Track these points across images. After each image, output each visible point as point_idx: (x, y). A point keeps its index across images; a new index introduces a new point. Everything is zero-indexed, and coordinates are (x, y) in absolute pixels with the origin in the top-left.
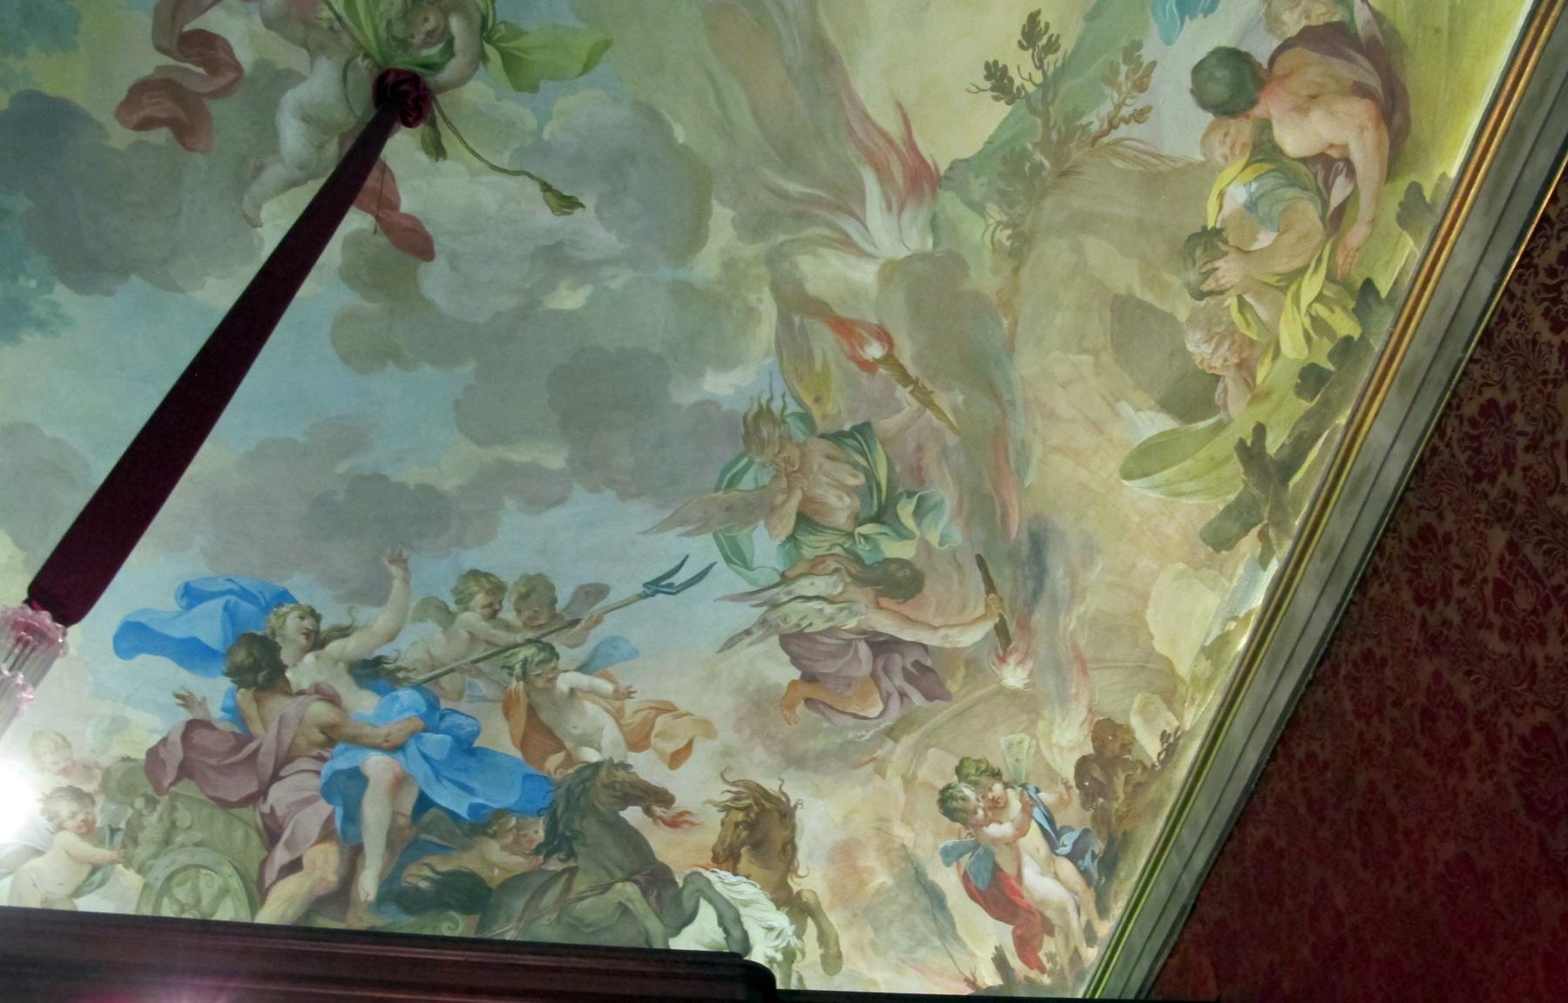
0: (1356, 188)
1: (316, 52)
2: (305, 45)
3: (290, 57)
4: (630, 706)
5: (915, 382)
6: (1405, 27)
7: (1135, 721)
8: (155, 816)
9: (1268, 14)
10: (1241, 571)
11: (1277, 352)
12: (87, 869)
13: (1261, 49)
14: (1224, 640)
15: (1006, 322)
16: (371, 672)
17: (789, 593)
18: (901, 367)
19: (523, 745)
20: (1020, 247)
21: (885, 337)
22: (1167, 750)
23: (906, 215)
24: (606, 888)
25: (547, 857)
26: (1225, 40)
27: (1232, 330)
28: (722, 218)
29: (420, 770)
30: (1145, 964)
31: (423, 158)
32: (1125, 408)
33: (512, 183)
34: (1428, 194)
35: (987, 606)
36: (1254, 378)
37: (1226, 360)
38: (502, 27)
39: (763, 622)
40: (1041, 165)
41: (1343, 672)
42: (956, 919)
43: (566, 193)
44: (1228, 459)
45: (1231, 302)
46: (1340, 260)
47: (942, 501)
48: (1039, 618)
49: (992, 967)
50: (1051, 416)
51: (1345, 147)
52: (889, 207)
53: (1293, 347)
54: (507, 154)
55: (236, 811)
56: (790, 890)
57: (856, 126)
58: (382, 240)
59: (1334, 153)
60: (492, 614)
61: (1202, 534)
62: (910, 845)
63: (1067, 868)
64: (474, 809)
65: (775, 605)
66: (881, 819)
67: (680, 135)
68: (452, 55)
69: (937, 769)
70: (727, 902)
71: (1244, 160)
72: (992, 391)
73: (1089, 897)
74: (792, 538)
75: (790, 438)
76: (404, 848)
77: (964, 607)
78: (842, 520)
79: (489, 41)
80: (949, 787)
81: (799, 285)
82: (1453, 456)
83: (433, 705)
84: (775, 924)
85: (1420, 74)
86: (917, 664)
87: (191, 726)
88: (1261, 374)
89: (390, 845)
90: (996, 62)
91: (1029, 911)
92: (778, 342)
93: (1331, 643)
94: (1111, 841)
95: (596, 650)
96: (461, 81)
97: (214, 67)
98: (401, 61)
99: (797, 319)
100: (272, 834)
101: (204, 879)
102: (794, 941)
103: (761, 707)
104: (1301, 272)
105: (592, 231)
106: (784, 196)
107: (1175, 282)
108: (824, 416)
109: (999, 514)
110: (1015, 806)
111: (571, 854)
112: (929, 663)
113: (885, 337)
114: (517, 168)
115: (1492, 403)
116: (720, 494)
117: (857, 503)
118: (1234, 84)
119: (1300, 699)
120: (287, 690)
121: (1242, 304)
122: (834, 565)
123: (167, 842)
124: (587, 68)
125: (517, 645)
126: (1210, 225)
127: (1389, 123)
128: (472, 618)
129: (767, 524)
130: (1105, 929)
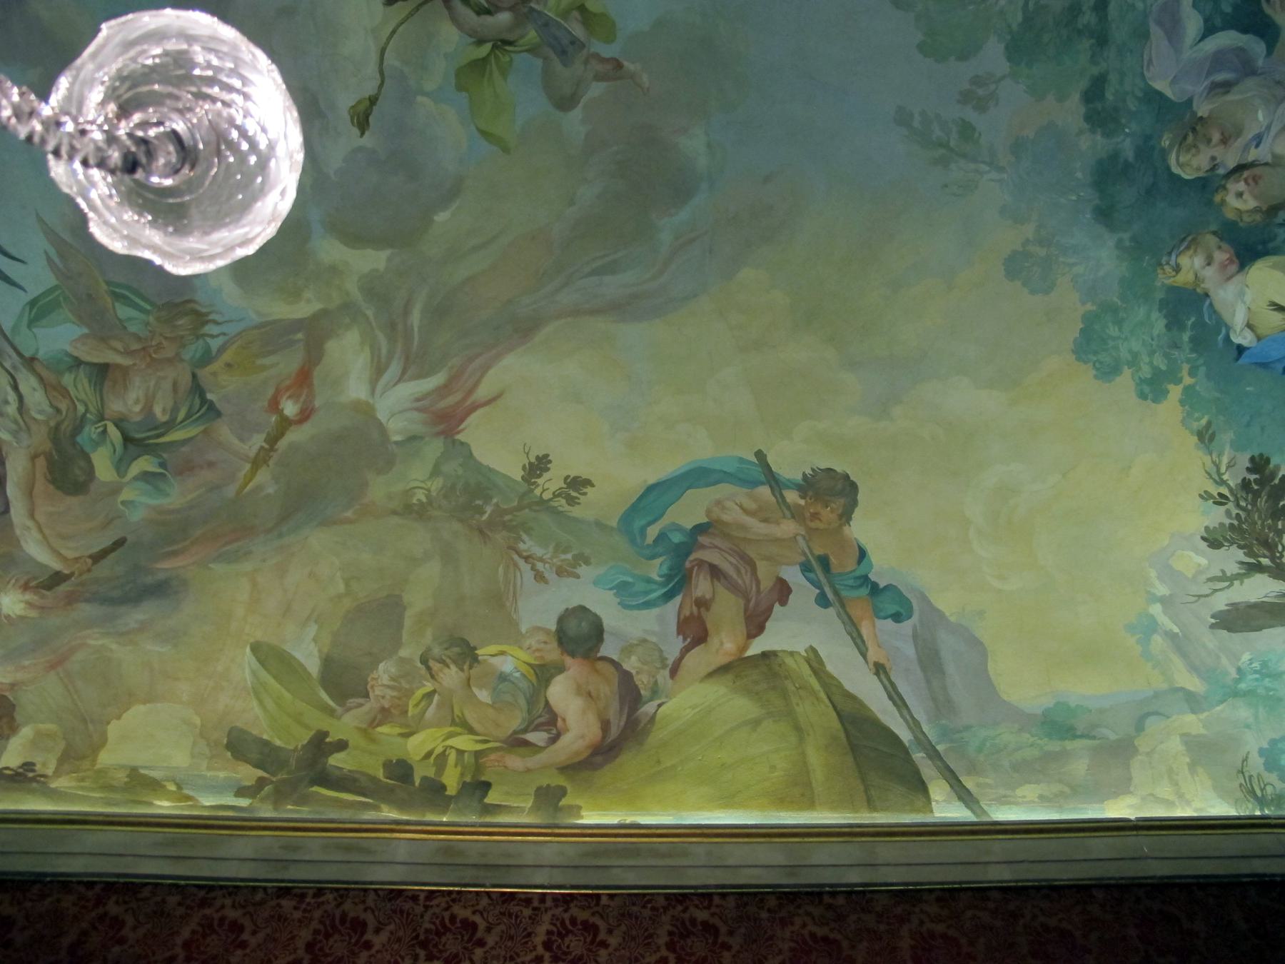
0: (545, 748)
5: (272, 449)
7: (26, 732)
9: (632, 646)
10: (222, 774)
11: (407, 735)
13: (609, 649)
14: (155, 786)
15: (349, 514)
17: (14, 367)
18: (282, 434)
20: (415, 512)
21: (305, 415)
22: (18, 774)
23: (416, 415)
26: (607, 622)
27: (409, 693)
28: (373, 260)
32: (312, 629)
33: (371, 68)
34: (563, 802)
35: (77, 560)
36: (379, 725)
37: (383, 697)
38: (508, 59)
41: (207, 911)
43: (371, 119)
44: (307, 727)
45: (429, 686)
46: (493, 757)
47: (168, 495)
51: (567, 730)
52: (418, 400)
53: (417, 746)
54: (397, 64)
59: (560, 723)
67: (441, 217)
71: (533, 662)
74: (78, 363)
75: (184, 346)
78: (115, 406)
82: (422, 916)
85: (630, 763)
88: (384, 729)
90: (550, 462)
92: (274, 322)
93: (221, 887)
96: (455, 20)
99: (300, 336)
104: (471, 731)
106: (406, 312)
108: (214, 374)
109: (175, 547)
115: (474, 926)
116: (104, 287)
117: (138, 419)
118: (580, 637)
119: (157, 886)
121: (430, 695)
122: (63, 406)
124: (484, 133)
129: (85, 336)
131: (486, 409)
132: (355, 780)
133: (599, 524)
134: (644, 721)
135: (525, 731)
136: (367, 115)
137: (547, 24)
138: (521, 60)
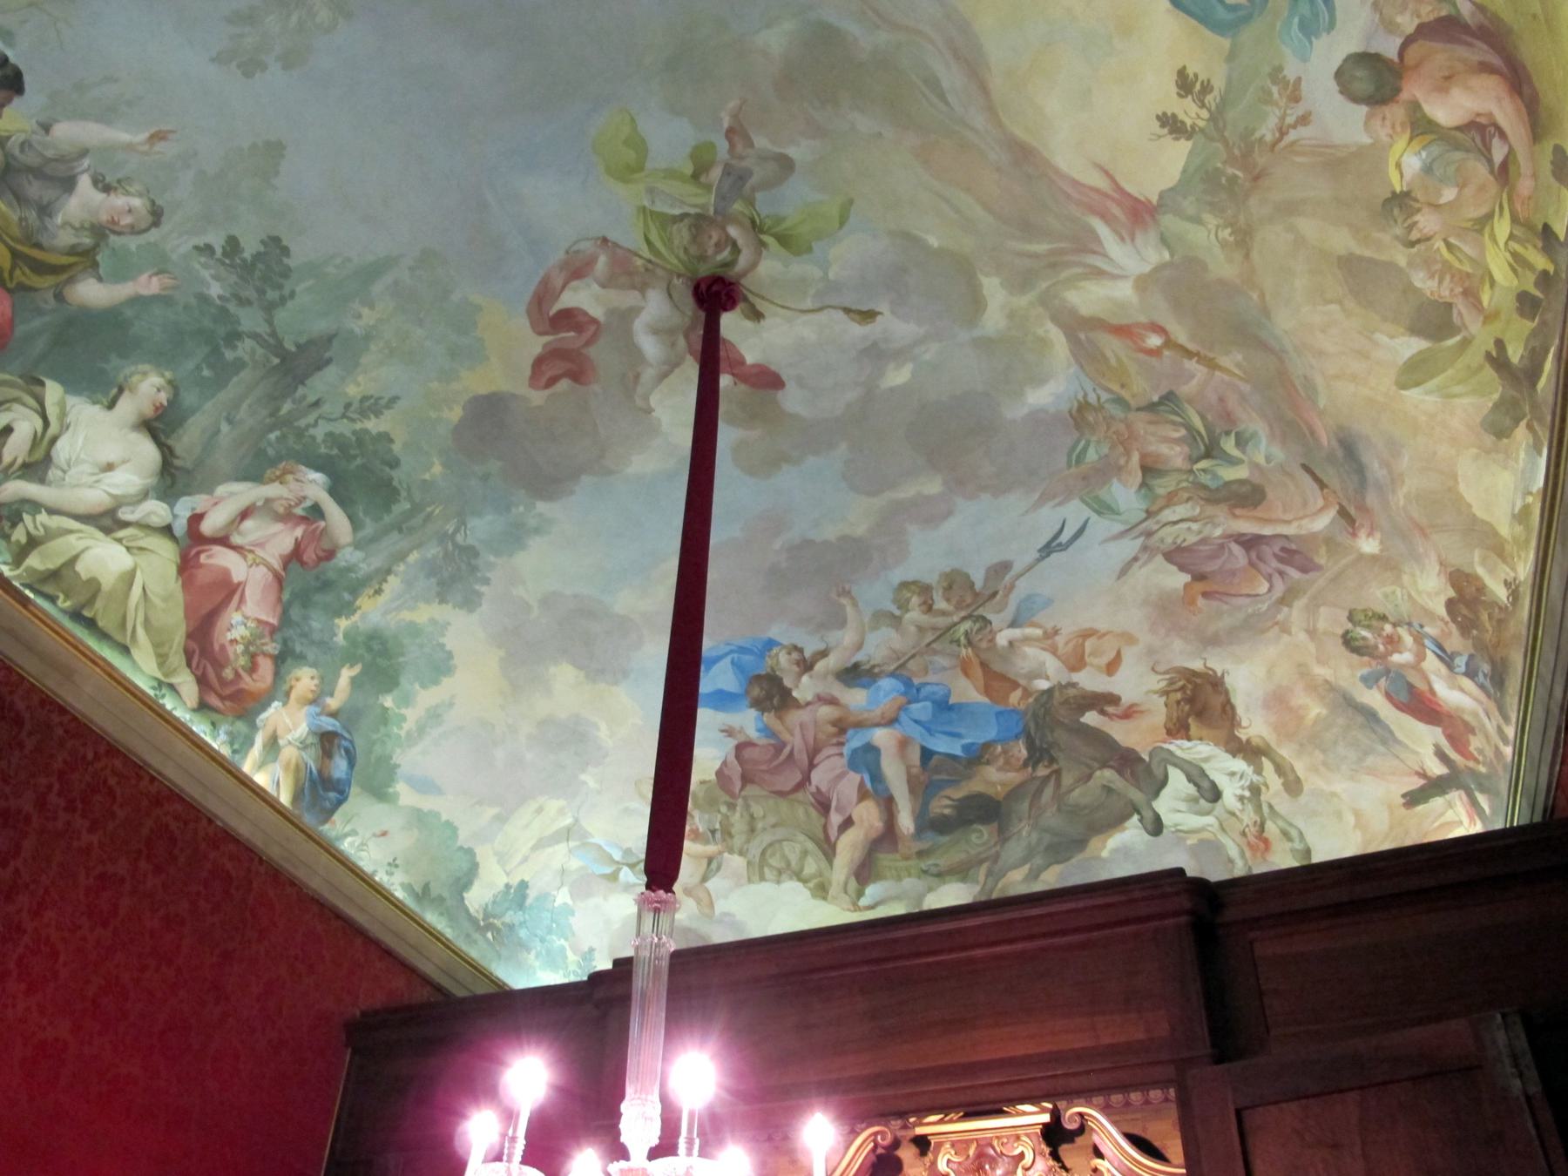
1: (642, 288)
2: (633, 287)
3: (630, 298)
4: (1060, 640)
5: (1198, 354)
6: (1507, 15)
7: (1480, 571)
8: (738, 815)
9: (1382, 19)
10: (1522, 455)
11: (1493, 283)
12: (705, 862)
14: (1526, 509)
15: (1255, 296)
16: (853, 674)
19: (987, 691)
20: (1243, 239)
21: (1159, 329)
24: (1089, 777)
25: (1034, 769)
26: (1354, 47)
27: (1447, 267)
28: (993, 288)
29: (916, 733)
30: (1545, 770)
31: (748, 324)
33: (823, 317)
36: (1480, 303)
39: (1145, 548)
40: (1236, 176)
42: (1392, 727)
43: (864, 308)
44: (1481, 368)
48: (1371, 499)
49: (1436, 760)
50: (1321, 353)
51: (1490, 115)
52: (1122, 239)
55: (793, 796)
56: (1239, 739)
57: (1070, 190)
58: (742, 387)
59: (1483, 120)
60: (929, 608)
61: (1482, 424)
62: (1331, 679)
63: (1467, 683)
64: (966, 748)
65: (1149, 534)
66: (1300, 665)
67: (934, 242)
68: (739, 251)
69: (1331, 620)
70: (1189, 763)
71: (1407, 136)
72: (1264, 346)
73: (1492, 706)
74: (1144, 484)
76: (923, 789)
77: (1305, 504)
78: (1179, 462)
79: (762, 232)
80: (1347, 632)
81: (1073, 312)
83: (908, 683)
84: (1235, 769)
86: (1283, 549)
87: (739, 748)
88: (1485, 299)
89: (912, 791)
90: (1165, 114)
91: (1450, 716)
92: (1074, 355)
94: (1493, 662)
95: (1018, 609)
96: (754, 265)
97: (579, 328)
98: (704, 270)
99: (1082, 336)
100: (824, 806)
101: (787, 847)
102: (1256, 778)
103: (1165, 610)
104: (1489, 216)
105: (894, 327)
107: (1386, 238)
108: (1133, 396)
110: (1408, 640)
111: (1052, 760)
112: (1294, 547)
113: (1159, 329)
114: (818, 305)
116: (1073, 470)
117: (1186, 449)
118: (1374, 80)
120: (797, 705)
121: (1449, 246)
122: (1186, 495)
123: (752, 830)
125: (955, 624)
126: (1398, 190)
127: (1520, 94)
128: (915, 615)
129: (1120, 480)
130: (1510, 731)
131: (1118, 179)
132: (1533, 349)
133: (1231, 57)
134: (1480, 18)
135: (1490, 161)
136: (860, 313)
137: (721, 197)
138: (764, 206)
